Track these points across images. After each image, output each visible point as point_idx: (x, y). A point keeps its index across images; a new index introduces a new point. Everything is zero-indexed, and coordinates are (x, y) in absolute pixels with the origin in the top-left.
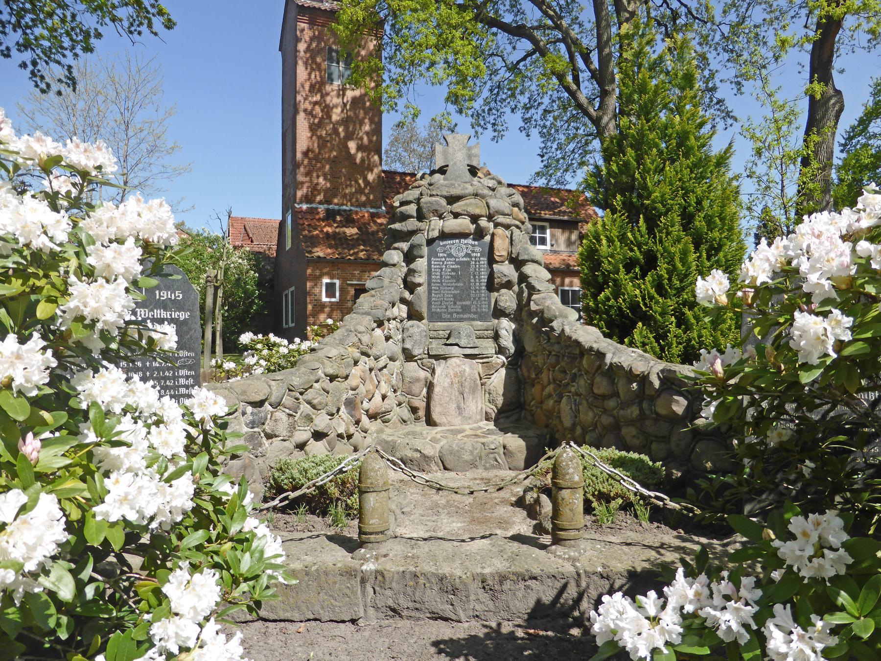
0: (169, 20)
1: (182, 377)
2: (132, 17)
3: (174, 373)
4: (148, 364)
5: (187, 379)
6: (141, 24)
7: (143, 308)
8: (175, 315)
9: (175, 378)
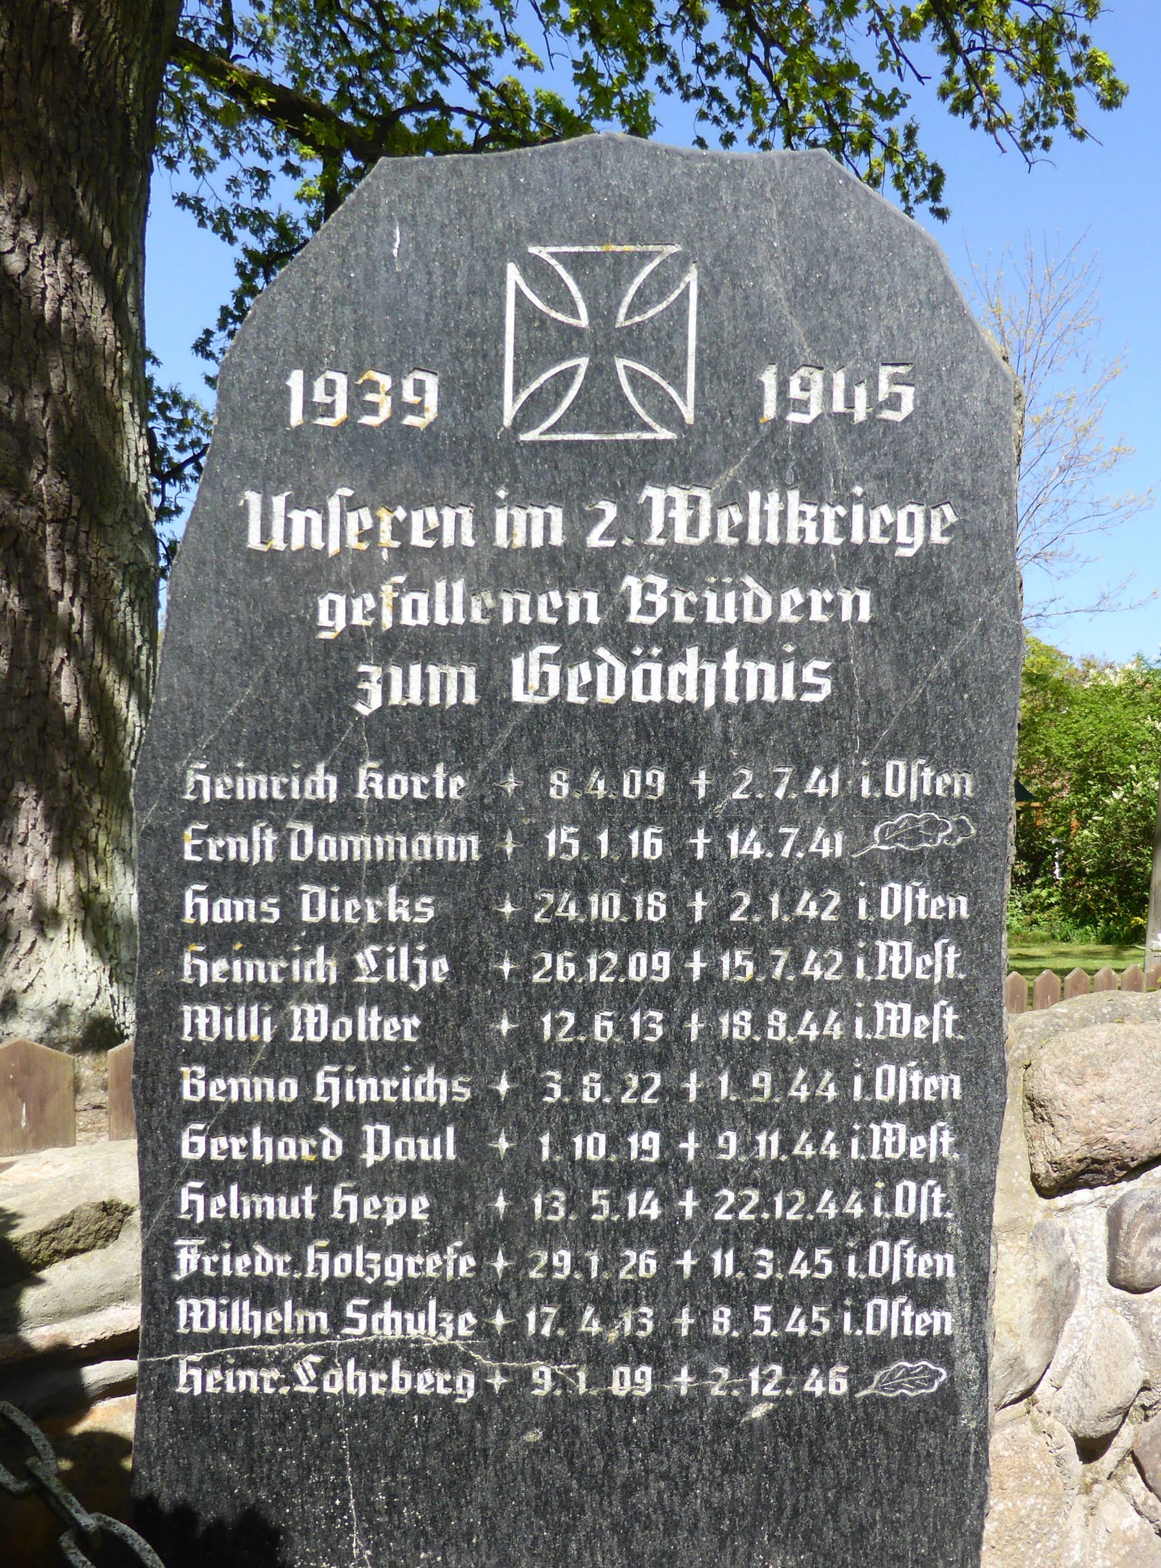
0: (1113, 85)
1: (896, 930)
2: (1032, 108)
3: (848, 907)
4: (701, 840)
5: (924, 946)
6: (1051, 122)
7: (685, 481)
8: (869, 525)
9: (854, 935)
